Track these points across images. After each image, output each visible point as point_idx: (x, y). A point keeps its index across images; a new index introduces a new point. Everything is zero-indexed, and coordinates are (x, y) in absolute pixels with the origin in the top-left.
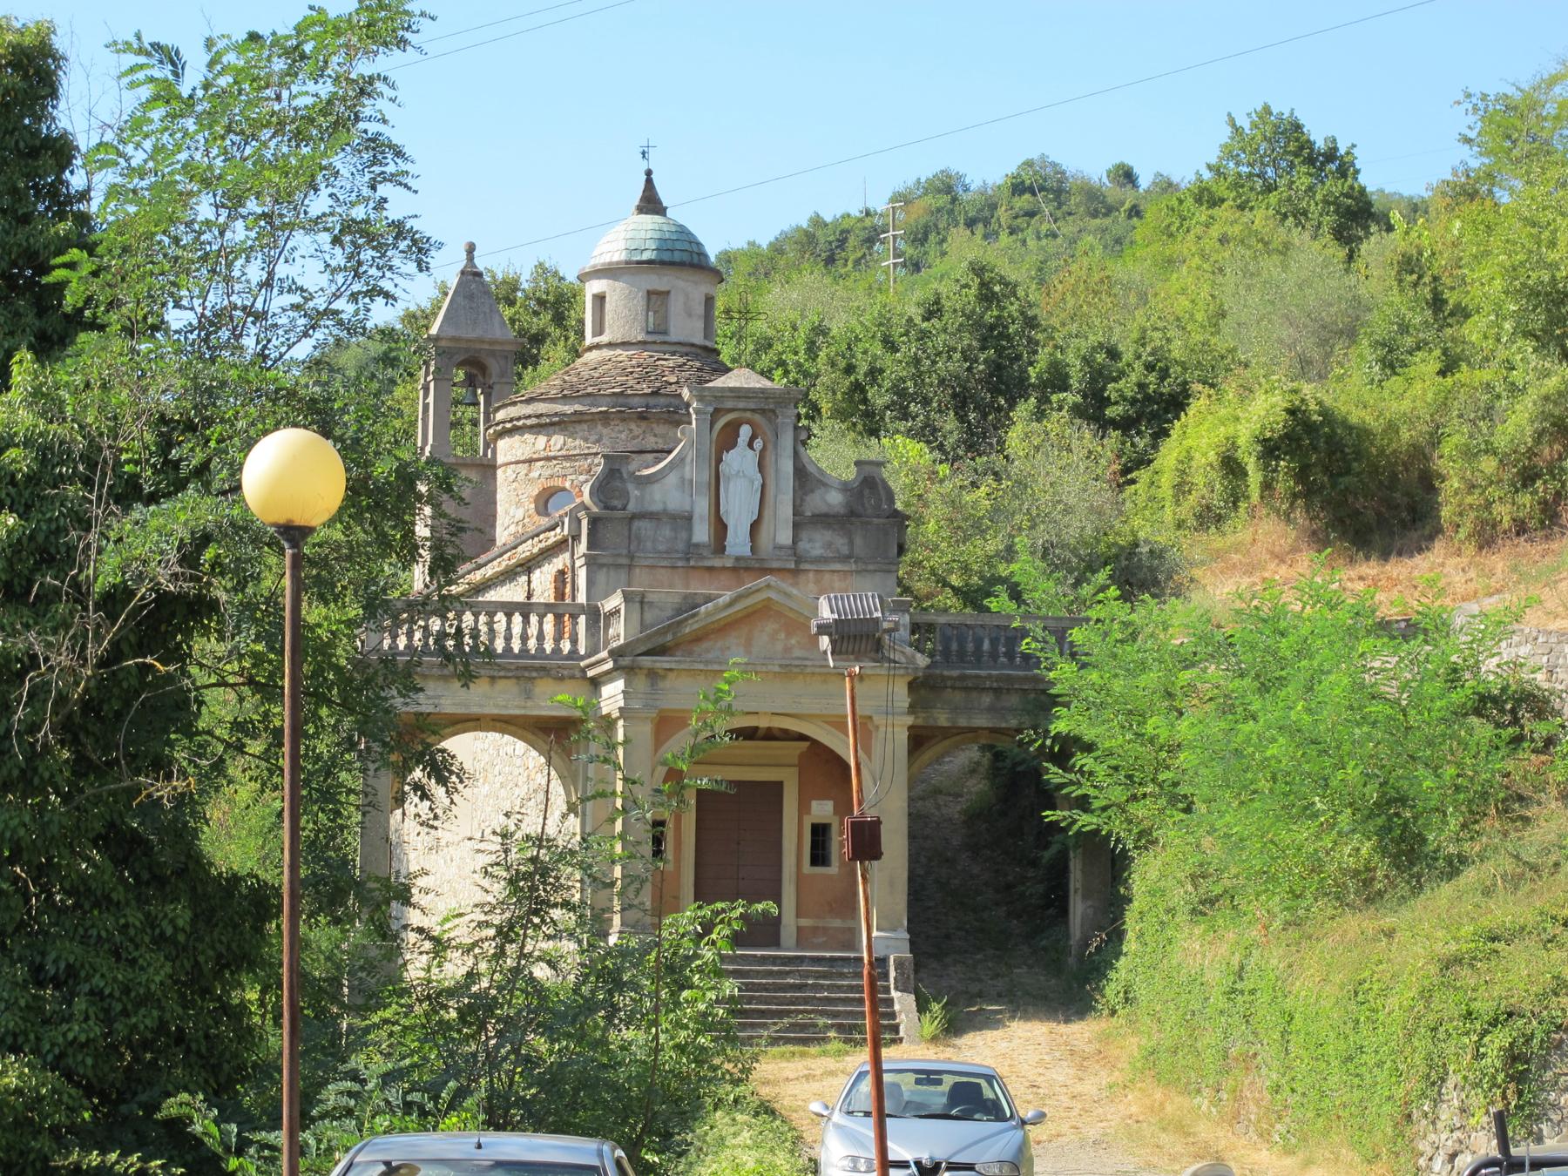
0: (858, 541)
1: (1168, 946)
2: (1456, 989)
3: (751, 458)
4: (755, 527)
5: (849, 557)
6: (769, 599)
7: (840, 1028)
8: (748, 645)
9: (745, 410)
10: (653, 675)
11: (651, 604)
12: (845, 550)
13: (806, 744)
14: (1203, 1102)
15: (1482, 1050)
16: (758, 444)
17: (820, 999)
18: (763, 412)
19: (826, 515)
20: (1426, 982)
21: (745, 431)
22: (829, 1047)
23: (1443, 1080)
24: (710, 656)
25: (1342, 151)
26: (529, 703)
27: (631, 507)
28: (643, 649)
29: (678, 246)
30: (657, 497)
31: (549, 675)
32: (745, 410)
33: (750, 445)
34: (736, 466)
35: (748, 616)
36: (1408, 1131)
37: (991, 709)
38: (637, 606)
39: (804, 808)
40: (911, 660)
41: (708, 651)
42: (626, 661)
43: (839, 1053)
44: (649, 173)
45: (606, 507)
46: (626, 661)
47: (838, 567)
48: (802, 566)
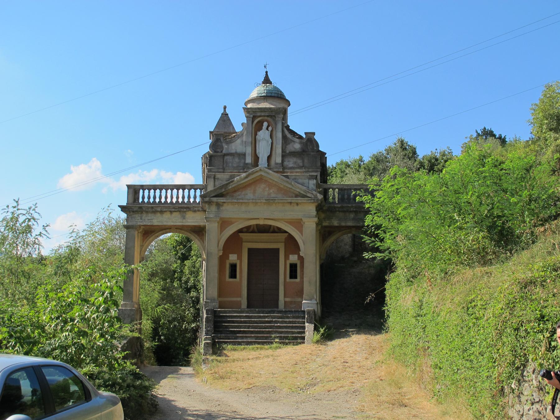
0: (306, 161)
1: (400, 297)
2: (532, 300)
3: (268, 133)
4: (269, 158)
5: (303, 167)
6: (261, 175)
7: (281, 338)
8: (254, 192)
9: (264, 116)
10: (218, 205)
11: (218, 179)
12: (301, 164)
13: (287, 234)
14: (410, 371)
15: (553, 344)
16: (270, 129)
17: (276, 326)
18: (270, 116)
19: (294, 152)
20: (511, 297)
21: (265, 124)
22: (272, 346)
23: (525, 366)
24: (240, 197)
25: (503, 137)
26: (184, 221)
27: (224, 152)
28: (213, 195)
29: (274, 92)
30: (233, 148)
31: (190, 210)
32: (264, 116)
33: (267, 129)
34: (262, 136)
35: (254, 182)
36: (501, 401)
37: (354, 219)
38: (213, 179)
39: (286, 258)
40: (316, 196)
41: (239, 195)
42: (207, 199)
43: (277, 348)
44: (267, 72)
45: (215, 152)
46: (207, 199)
47: (298, 170)
48: (285, 171)
